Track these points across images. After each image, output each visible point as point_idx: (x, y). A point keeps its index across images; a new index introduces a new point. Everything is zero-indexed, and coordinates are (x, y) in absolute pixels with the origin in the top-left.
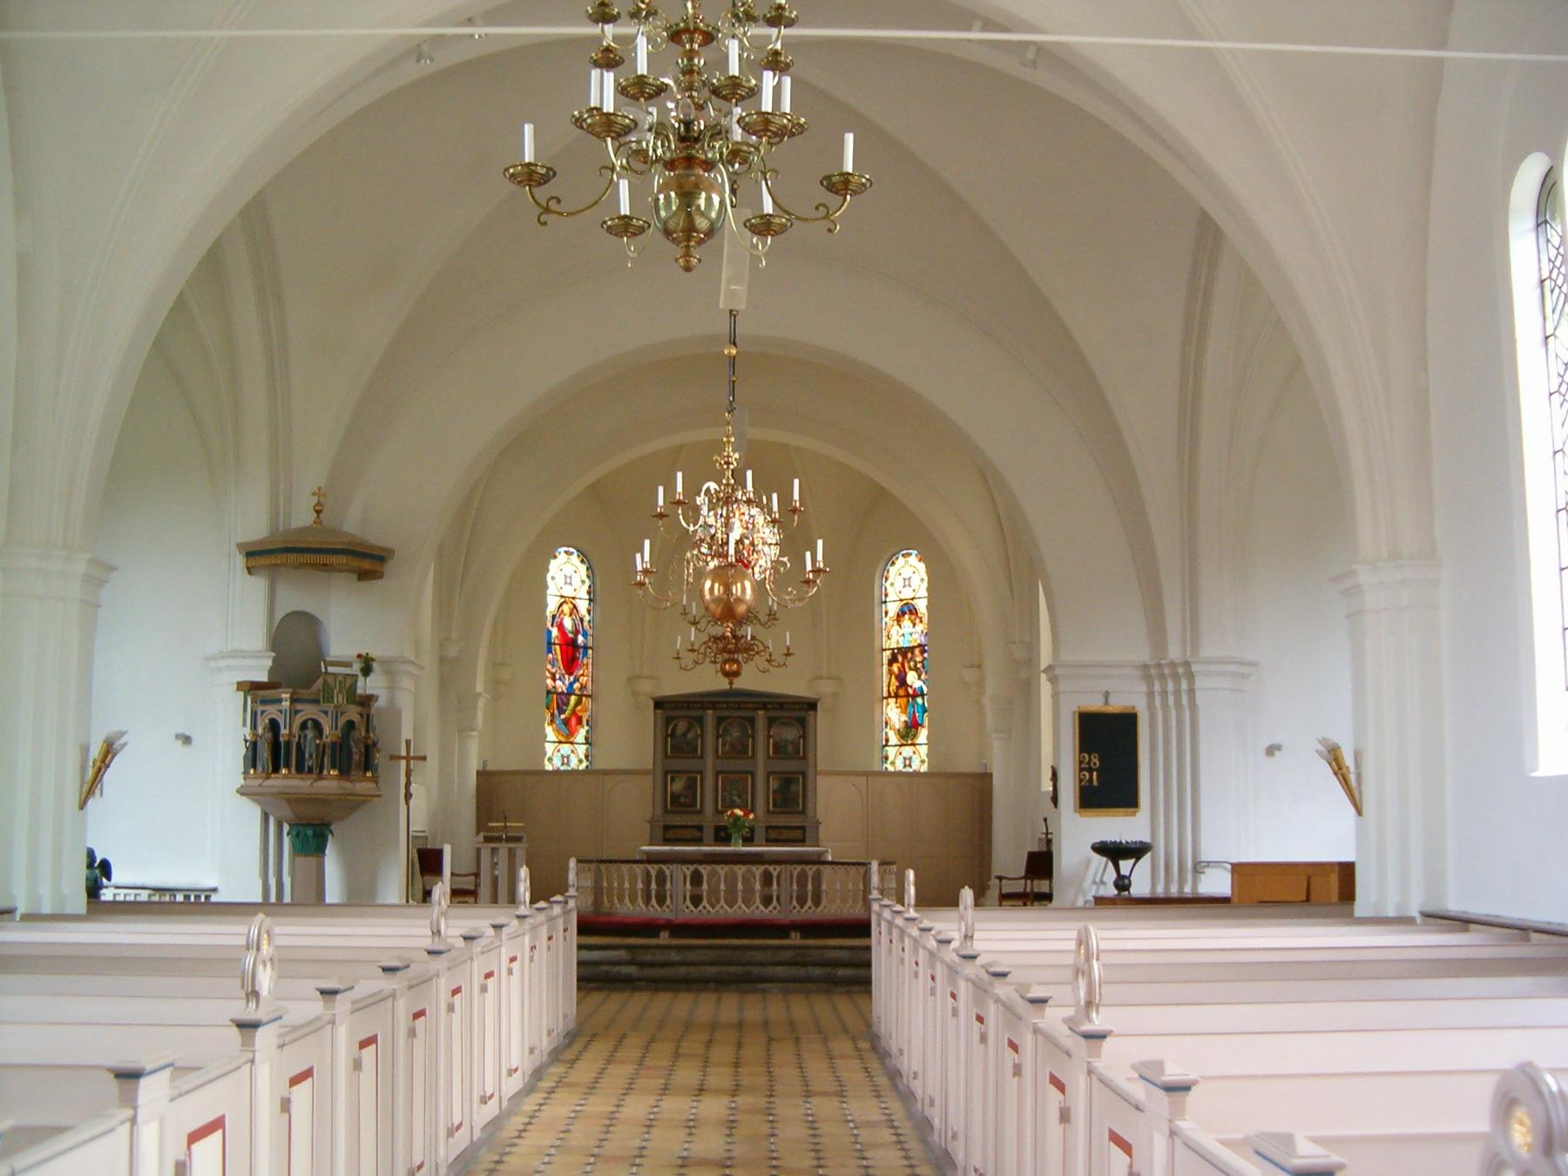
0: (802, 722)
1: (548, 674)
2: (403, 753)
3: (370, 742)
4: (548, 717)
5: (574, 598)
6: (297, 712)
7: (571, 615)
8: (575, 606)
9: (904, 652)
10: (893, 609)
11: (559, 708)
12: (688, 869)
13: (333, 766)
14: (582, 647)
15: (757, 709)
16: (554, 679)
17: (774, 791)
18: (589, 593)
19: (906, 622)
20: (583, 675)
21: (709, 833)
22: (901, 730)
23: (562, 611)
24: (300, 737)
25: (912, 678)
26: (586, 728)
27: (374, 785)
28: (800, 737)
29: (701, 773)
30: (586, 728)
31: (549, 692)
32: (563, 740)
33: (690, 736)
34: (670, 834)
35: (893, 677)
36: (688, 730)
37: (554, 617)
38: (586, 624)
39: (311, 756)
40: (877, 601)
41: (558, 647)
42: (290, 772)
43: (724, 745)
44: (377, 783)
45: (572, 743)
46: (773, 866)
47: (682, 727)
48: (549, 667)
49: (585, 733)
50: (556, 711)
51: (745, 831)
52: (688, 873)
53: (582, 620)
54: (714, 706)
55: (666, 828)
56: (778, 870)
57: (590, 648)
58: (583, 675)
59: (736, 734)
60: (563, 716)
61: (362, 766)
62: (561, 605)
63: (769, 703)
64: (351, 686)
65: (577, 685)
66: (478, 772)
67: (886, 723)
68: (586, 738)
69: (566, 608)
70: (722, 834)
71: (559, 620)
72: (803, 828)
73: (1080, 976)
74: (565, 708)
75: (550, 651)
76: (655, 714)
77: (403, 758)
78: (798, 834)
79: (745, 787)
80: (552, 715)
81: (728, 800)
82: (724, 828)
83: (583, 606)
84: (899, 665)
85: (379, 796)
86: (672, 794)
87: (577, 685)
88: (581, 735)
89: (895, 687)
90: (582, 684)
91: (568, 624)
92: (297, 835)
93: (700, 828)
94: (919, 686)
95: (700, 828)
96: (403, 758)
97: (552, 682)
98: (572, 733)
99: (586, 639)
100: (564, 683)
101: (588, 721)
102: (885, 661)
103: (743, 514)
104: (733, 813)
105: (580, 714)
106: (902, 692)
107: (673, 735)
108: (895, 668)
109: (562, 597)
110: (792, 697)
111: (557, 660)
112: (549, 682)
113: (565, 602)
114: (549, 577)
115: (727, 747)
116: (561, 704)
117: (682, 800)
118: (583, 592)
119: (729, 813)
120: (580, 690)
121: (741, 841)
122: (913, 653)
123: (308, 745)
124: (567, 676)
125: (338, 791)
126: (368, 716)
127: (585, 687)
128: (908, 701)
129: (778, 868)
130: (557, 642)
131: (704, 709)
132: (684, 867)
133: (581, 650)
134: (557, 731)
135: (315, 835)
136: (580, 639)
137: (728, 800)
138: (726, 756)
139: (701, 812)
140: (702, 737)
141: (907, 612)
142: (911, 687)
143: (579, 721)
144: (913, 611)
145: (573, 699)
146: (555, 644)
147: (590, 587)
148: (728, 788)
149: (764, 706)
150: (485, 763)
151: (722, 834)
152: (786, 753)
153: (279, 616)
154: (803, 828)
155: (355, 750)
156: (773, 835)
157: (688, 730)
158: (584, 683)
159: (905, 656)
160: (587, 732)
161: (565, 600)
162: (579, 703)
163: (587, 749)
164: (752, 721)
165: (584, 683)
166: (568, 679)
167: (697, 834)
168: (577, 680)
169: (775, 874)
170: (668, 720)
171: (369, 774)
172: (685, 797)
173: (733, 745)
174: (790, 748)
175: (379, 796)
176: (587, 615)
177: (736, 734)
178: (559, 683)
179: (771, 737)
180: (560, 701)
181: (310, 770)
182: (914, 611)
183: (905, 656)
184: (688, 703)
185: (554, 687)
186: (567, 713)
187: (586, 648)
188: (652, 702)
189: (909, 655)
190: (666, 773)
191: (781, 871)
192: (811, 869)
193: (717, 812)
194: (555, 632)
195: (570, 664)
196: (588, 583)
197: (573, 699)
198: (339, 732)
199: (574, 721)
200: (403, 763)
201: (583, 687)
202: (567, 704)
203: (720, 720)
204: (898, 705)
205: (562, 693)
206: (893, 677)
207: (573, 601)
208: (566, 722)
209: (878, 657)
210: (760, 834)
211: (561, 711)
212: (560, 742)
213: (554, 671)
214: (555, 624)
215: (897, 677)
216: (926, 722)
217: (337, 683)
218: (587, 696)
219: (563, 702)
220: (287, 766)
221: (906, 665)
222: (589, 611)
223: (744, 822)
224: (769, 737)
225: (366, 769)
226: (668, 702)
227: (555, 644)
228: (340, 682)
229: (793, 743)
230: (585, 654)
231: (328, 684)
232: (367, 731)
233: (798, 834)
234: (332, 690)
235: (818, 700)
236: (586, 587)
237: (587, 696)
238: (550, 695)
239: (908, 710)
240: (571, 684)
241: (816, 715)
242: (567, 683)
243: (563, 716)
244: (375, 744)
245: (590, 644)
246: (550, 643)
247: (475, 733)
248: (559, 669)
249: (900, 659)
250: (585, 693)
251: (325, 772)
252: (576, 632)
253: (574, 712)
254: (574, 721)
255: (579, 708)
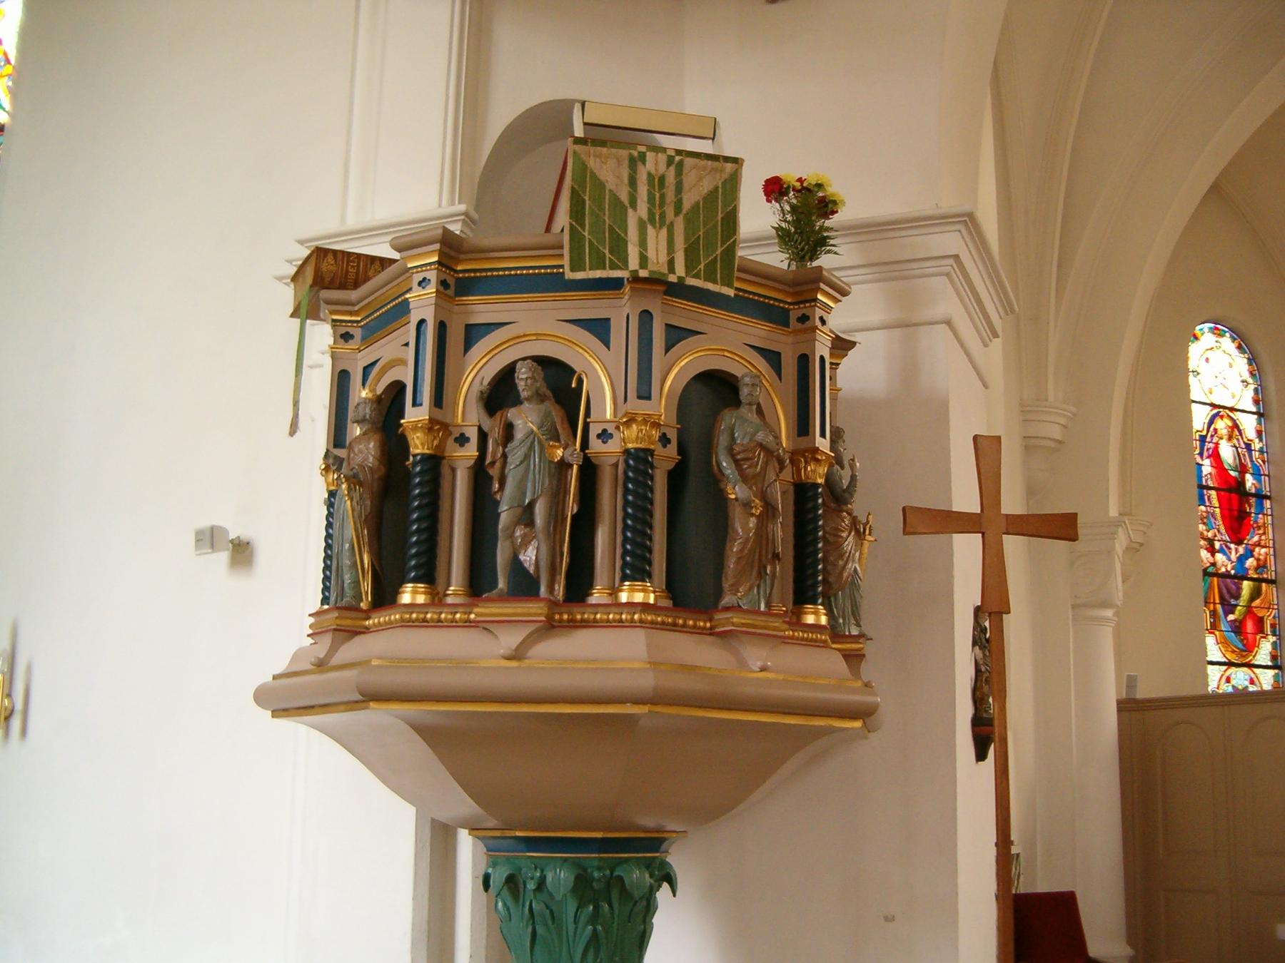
2: (966, 499)
3: (817, 474)
5: (1232, 409)
6: (473, 334)
7: (1230, 438)
11: (1223, 601)
13: (637, 570)
16: (1212, 551)
18: (1256, 402)
20: (1258, 544)
23: (1216, 430)
24: (483, 436)
26: (1272, 639)
27: (841, 665)
30: (1272, 639)
31: (1206, 573)
32: (1233, 658)
38: (1256, 455)
39: (526, 515)
41: (1213, 493)
42: (437, 599)
44: (854, 659)
45: (1250, 666)
48: (1202, 527)
50: (1219, 607)
53: (1248, 447)
58: (1258, 544)
60: (1231, 617)
61: (783, 571)
62: (1211, 422)
64: (711, 196)
65: (1250, 562)
66: (1119, 703)
68: (1274, 657)
69: (1222, 425)
71: (1211, 445)
74: (1233, 602)
75: (1202, 501)
77: (966, 523)
80: (1214, 614)
83: (1249, 424)
85: (865, 713)
88: (1263, 653)
90: (1258, 560)
91: (1227, 453)
92: (512, 882)
96: (966, 523)
97: (1209, 555)
98: (1250, 648)
99: (1260, 481)
100: (1229, 559)
101: (1273, 626)
109: (1213, 406)
111: (1213, 515)
112: (1204, 554)
116: (1227, 597)
118: (1245, 399)
120: (1256, 569)
123: (515, 458)
125: (646, 682)
126: (804, 362)
127: (1264, 566)
130: (1210, 484)
133: (1253, 500)
134: (1223, 642)
135: (582, 885)
136: (1250, 481)
143: (1259, 623)
145: (1246, 586)
146: (1209, 488)
147: (1256, 390)
150: (1131, 682)
153: (503, 112)
155: (736, 491)
160: (1274, 644)
161: (1218, 411)
162: (1256, 594)
163: (1276, 676)
166: (1236, 551)
168: (1249, 553)
171: (815, 616)
175: (865, 713)
176: (1257, 441)
178: (1220, 557)
180: (1225, 591)
181: (524, 585)
185: (1214, 564)
186: (1237, 612)
187: (1260, 497)
194: (1207, 467)
195: (1238, 525)
197: (1246, 586)
198: (662, 406)
199: (1250, 627)
200: (967, 549)
201: (1261, 566)
202: (1237, 597)
205: (1227, 575)
208: (1238, 628)
211: (1229, 609)
212: (1230, 664)
213: (1210, 535)
214: (1205, 454)
217: (643, 190)
219: (1229, 591)
220: (428, 576)
222: (1259, 433)
225: (803, 595)
227: (1209, 488)
228: (657, 182)
230: (1261, 509)
231: (600, 185)
232: (803, 426)
234: (620, 210)
236: (1249, 392)
240: (1242, 559)
242: (1233, 557)
243: (1231, 617)
244: (838, 496)
245: (1266, 491)
246: (1201, 487)
247: (1109, 613)
248: (1219, 532)
251: (598, 596)
252: (1243, 469)
253: (1249, 610)
254: (1250, 627)
255: (1257, 603)
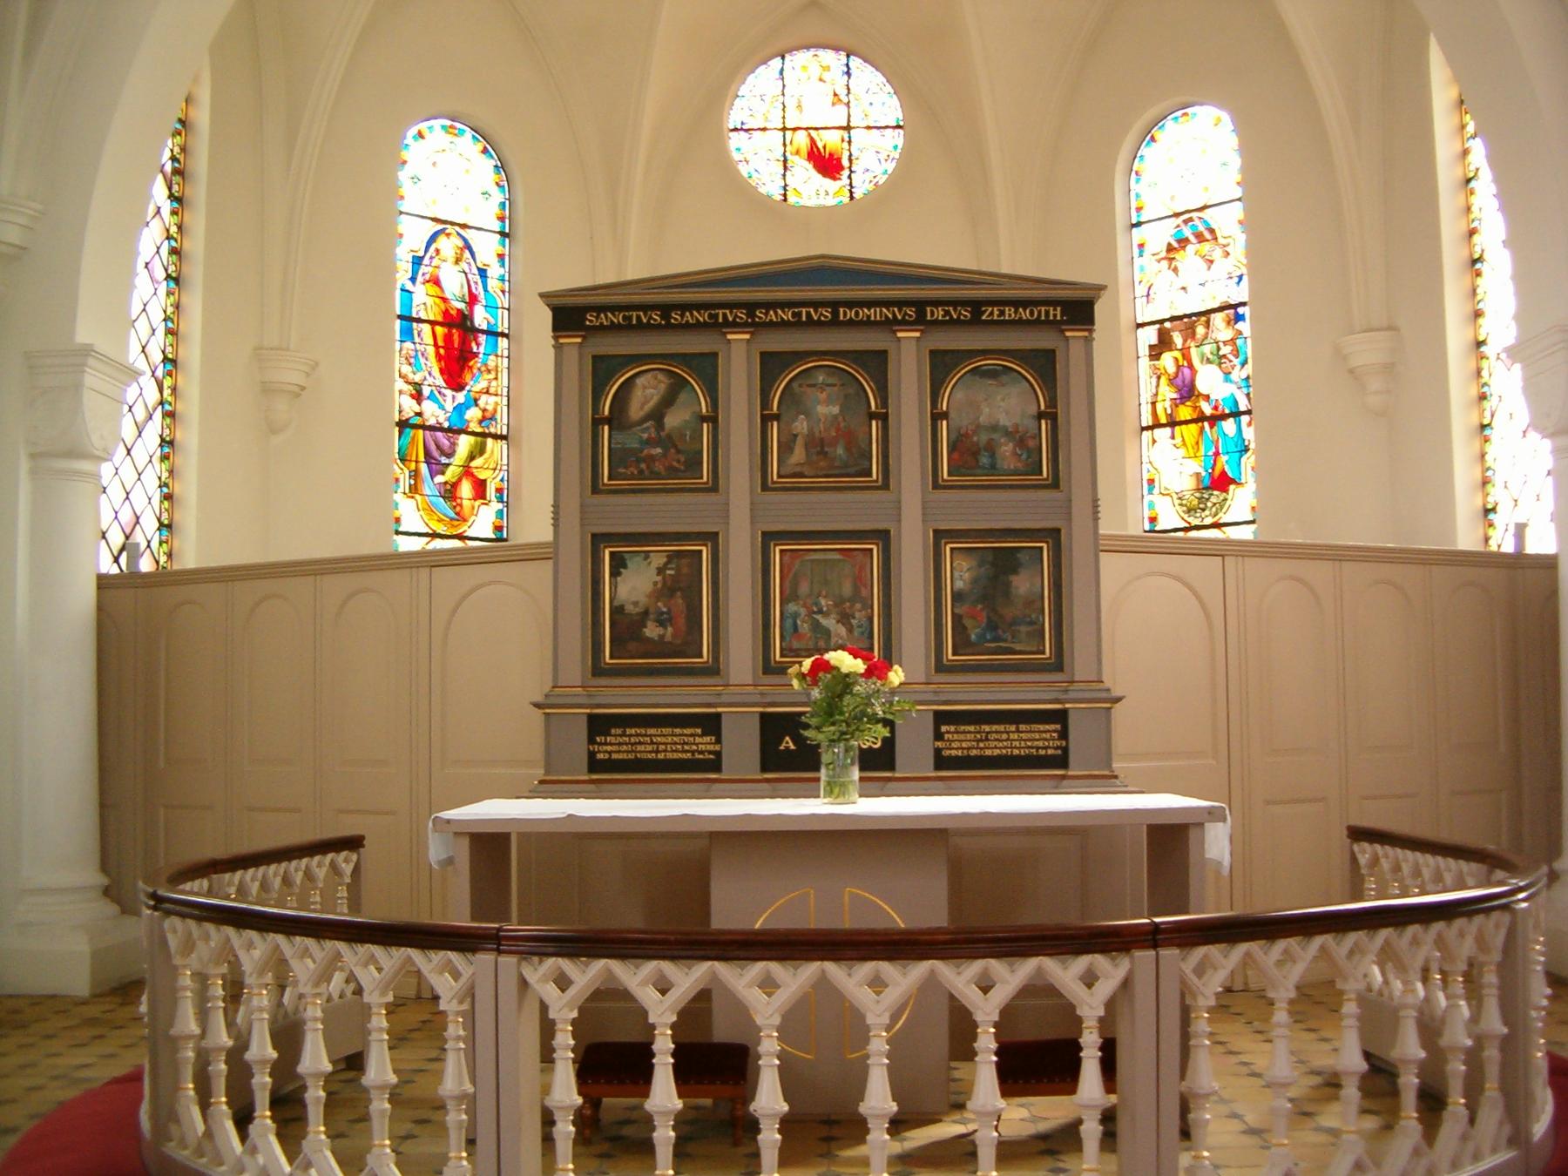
0: (1045, 366)
1: (400, 384)
4: (405, 481)
7: (458, 261)
8: (468, 246)
9: (1189, 322)
10: (1157, 236)
12: (563, 983)
14: (483, 332)
15: (890, 325)
17: (957, 597)
19: (1188, 259)
21: (741, 742)
22: (1187, 495)
25: (1209, 381)
26: (497, 506)
28: (1040, 416)
29: (711, 538)
31: (403, 425)
33: (673, 420)
34: (614, 746)
35: (1164, 380)
36: (668, 401)
37: (417, 261)
38: (493, 284)
40: (1120, 223)
43: (786, 448)
46: (1082, 962)
47: (647, 391)
49: (493, 518)
50: (424, 468)
51: (873, 737)
52: (564, 1011)
53: (483, 273)
54: (752, 316)
55: (599, 725)
56: (1106, 988)
57: (503, 335)
59: (826, 408)
62: (433, 238)
63: (936, 303)
67: (1151, 482)
69: (448, 245)
70: (788, 743)
72: (1060, 717)
73: (1226, 872)
74: (444, 460)
76: (558, 347)
78: (1042, 738)
79: (861, 581)
80: (415, 474)
81: (805, 628)
82: (791, 724)
83: (487, 248)
84: (1178, 354)
86: (617, 611)
87: (473, 414)
89: (1168, 404)
90: (484, 410)
93: (711, 724)
94: (1227, 394)
95: (711, 724)
101: (499, 490)
102: (1144, 351)
103: (827, 69)
104: (821, 666)
105: (482, 475)
106: (1185, 413)
107: (617, 420)
108: (1168, 361)
110: (730, 932)
113: (442, 231)
114: (404, 175)
115: (798, 455)
116: (436, 453)
117: (651, 631)
119: (807, 663)
120: (480, 422)
121: (856, 774)
122: (1207, 325)
124: (449, 393)
127: (492, 418)
128: (1202, 428)
129: (1111, 970)
131: (718, 327)
132: (539, 974)
137: (805, 628)
138: (794, 483)
139: (713, 670)
140: (713, 419)
141: (1192, 238)
142: (1207, 398)
144: (1208, 235)
145: (465, 443)
148: (804, 589)
149: (919, 314)
151: (788, 743)
152: (993, 468)
154: (1060, 717)
156: (960, 741)
157: (668, 401)
158: (490, 408)
159: (1189, 333)
162: (479, 451)
164: (876, 364)
165: (490, 408)
166: (452, 399)
167: (705, 743)
169: (1091, 1006)
170: (603, 369)
172: (661, 623)
173: (818, 446)
174: (1006, 449)
177: (826, 408)
179: (945, 415)
180: (433, 447)
182: (1207, 235)
183: (1189, 333)
184: (666, 309)
188: (547, 315)
189: (1200, 330)
190: (599, 540)
191: (1126, 984)
192: (1288, 957)
193: (771, 669)
196: (498, 196)
197: (465, 443)
199: (466, 489)
201: (487, 417)
203: (772, 365)
204: (1178, 440)
206: (1164, 380)
207: (462, 232)
209: (1126, 338)
210: (915, 749)
213: (417, 378)
215: (1171, 381)
216: (1248, 477)
218: (496, 437)
221: (1194, 353)
223: (867, 701)
224: (937, 417)
226: (600, 309)
229: (1013, 434)
233: (1042, 738)
235: (1102, 288)
237: (496, 437)
238: (409, 432)
239: (1202, 452)
240: (460, 409)
241: (1089, 341)
242: (449, 406)
243: (439, 479)
248: (431, 373)
249: (1178, 339)
250: (492, 430)
252: (473, 300)
253: (467, 472)
254: (466, 489)
